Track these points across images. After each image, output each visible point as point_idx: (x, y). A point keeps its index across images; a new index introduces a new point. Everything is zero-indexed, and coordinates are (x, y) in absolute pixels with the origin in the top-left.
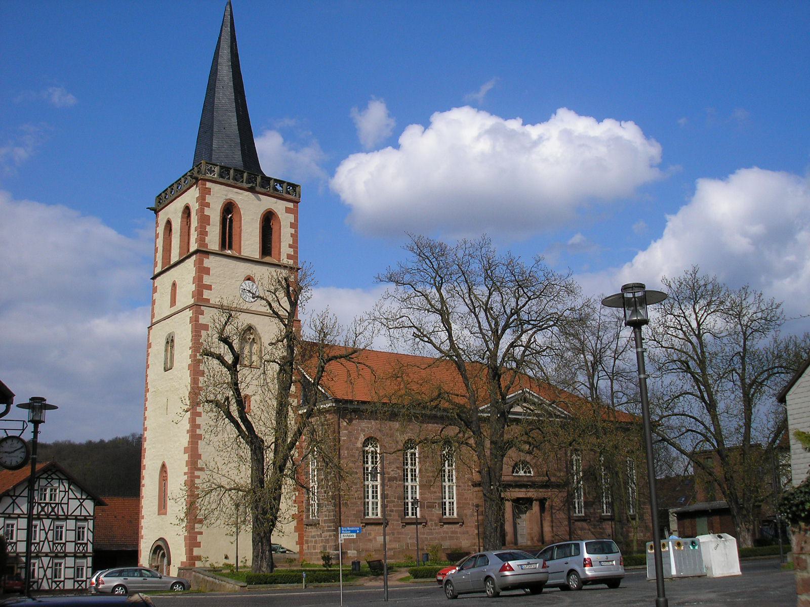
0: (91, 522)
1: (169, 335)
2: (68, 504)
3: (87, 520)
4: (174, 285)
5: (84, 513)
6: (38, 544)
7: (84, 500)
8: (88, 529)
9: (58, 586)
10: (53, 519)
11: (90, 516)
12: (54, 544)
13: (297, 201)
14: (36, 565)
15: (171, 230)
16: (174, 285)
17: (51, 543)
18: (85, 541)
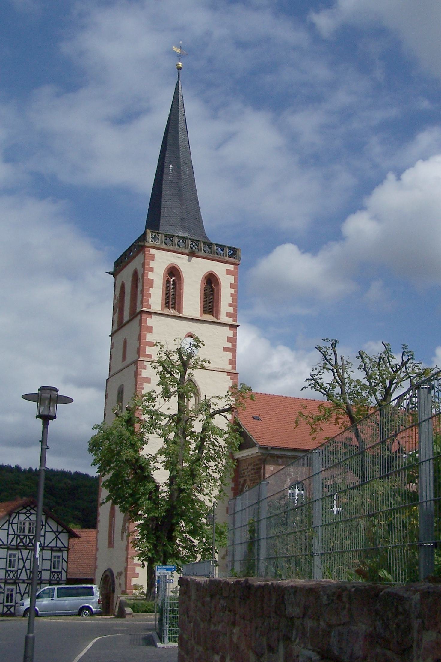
0: (65, 553)
1: (120, 386)
2: (44, 536)
3: (62, 551)
4: (125, 342)
5: (59, 545)
6: (17, 571)
7: (60, 533)
8: (63, 559)
9: (9, 610)
10: (30, 550)
11: (65, 547)
12: (51, 572)
13: (238, 263)
14: (14, 591)
15: (124, 293)
16: (125, 342)
17: (28, 571)
18: (60, 570)
